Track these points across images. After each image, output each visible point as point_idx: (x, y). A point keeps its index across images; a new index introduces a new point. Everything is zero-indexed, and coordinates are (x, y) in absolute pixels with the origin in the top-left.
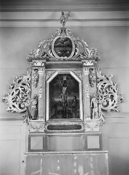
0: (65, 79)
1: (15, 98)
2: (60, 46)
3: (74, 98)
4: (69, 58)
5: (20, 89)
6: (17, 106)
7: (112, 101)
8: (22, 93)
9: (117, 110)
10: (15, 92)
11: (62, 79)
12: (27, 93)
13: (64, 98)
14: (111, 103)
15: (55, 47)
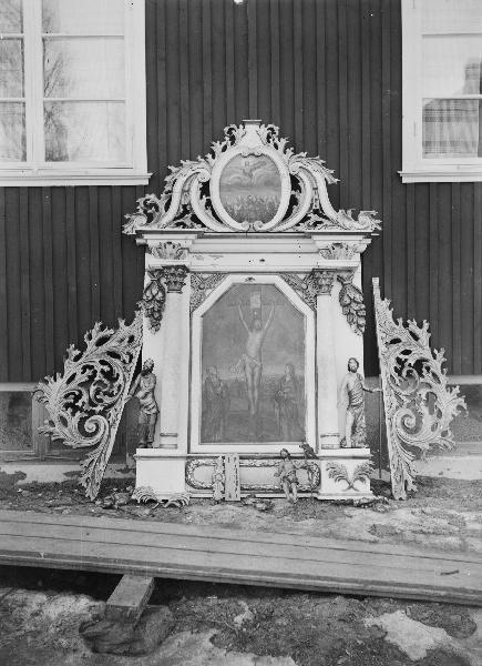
0: (255, 301)
1: (73, 393)
2: (240, 186)
3: (288, 371)
4: (266, 227)
5: (99, 367)
6: (74, 421)
7: (431, 412)
8: (100, 382)
9: (447, 444)
10: (79, 374)
11: (248, 303)
12: (116, 384)
13: (253, 369)
14: (428, 420)
15: (221, 187)
